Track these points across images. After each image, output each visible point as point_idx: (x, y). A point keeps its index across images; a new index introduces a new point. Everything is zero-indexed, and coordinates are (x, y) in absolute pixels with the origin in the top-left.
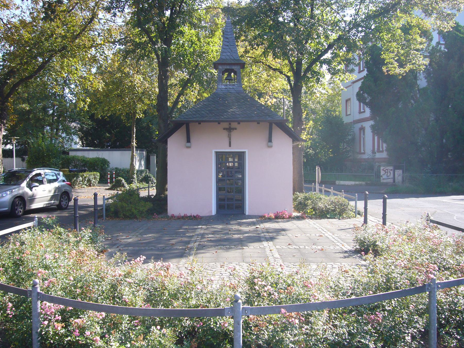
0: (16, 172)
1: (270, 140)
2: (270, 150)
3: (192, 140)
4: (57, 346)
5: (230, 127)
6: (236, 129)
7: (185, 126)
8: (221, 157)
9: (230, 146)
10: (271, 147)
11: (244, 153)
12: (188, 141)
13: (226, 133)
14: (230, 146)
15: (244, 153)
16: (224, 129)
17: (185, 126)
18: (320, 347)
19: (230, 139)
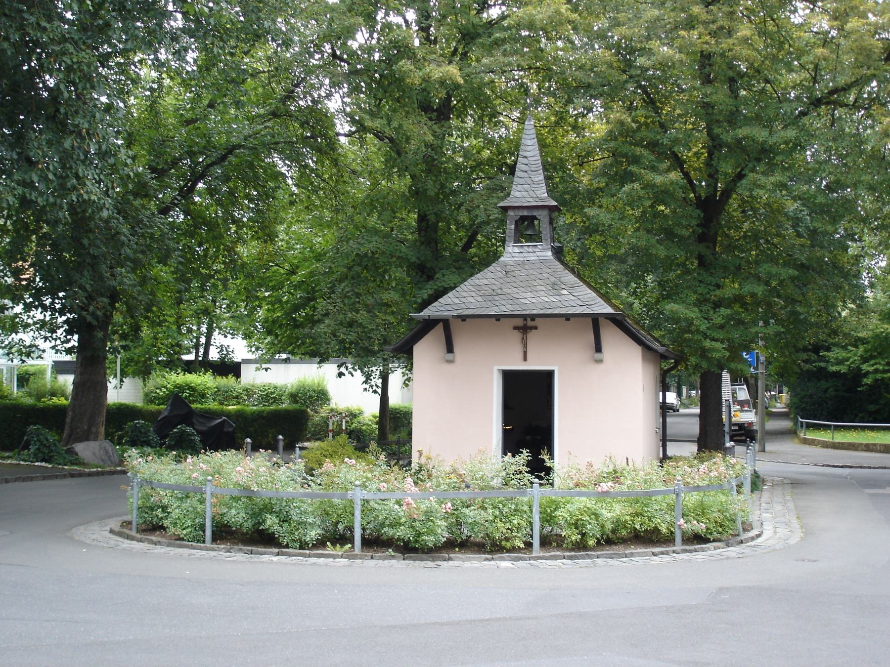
0: (419, 216)
1: (598, 349)
2: (600, 367)
3: (456, 349)
4: (597, 8)
5: (525, 325)
6: (536, 328)
7: (441, 325)
8: (511, 379)
9: (525, 359)
10: (600, 361)
11: (550, 374)
12: (450, 349)
13: (517, 335)
14: (525, 359)
15: (550, 374)
16: (515, 328)
17: (441, 325)
18: (475, 2)
19: (525, 346)
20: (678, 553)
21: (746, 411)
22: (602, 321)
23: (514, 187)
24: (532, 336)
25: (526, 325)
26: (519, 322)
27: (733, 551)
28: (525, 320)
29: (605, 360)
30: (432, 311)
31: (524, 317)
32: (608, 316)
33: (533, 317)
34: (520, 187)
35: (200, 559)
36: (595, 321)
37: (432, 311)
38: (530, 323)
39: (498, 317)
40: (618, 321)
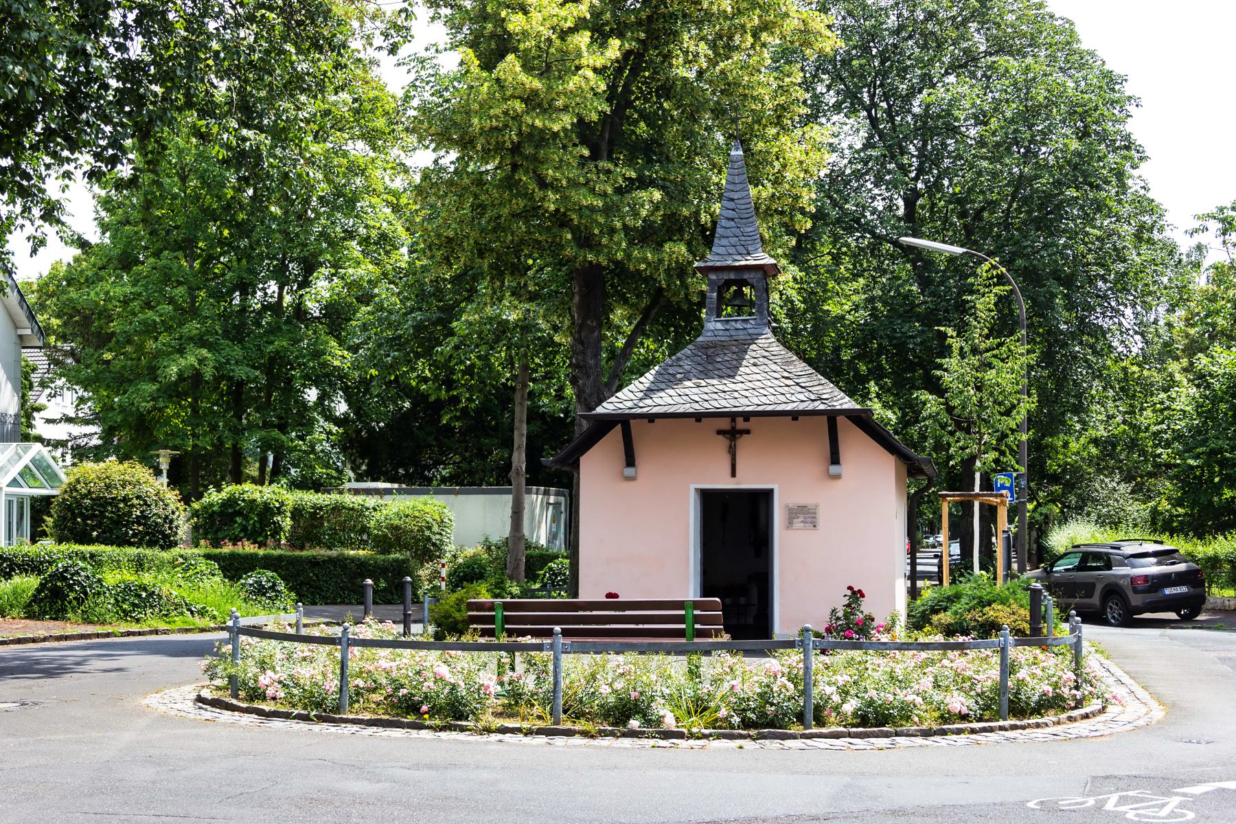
1: (835, 459)
6: (748, 432)
9: (733, 474)
12: (630, 461)
13: (723, 442)
14: (733, 474)
16: (719, 432)
20: (592, 737)
21: (633, 734)
22: (841, 420)
23: (716, 241)
24: (743, 443)
25: (734, 428)
26: (725, 424)
27: (1082, 727)
28: (733, 420)
29: (843, 476)
30: (607, 407)
31: (733, 416)
32: (851, 415)
33: (747, 416)
34: (724, 242)
35: (320, 734)
36: (832, 416)
37: (607, 407)
38: (741, 424)
39: (698, 417)
40: (862, 420)
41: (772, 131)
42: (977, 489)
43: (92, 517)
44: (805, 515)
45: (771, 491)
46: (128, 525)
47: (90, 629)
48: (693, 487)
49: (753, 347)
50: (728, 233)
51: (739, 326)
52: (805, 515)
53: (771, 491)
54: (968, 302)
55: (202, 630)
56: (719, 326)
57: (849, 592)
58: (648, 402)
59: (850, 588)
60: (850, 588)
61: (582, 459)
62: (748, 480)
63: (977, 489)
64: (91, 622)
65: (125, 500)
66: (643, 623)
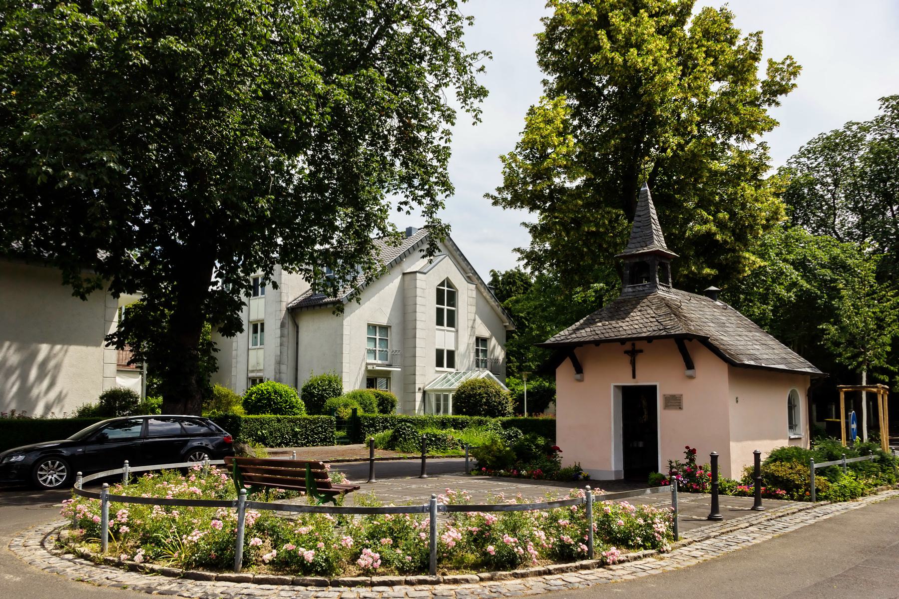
9: (634, 377)
13: (627, 358)
14: (634, 377)
25: (633, 349)
26: (628, 346)
34: (634, 241)
41: (422, 135)
42: (864, 384)
43: (464, 403)
44: (675, 402)
45: (655, 386)
46: (481, 406)
47: (402, 455)
48: (613, 384)
49: (645, 300)
50: (637, 235)
51: (641, 289)
52: (675, 402)
53: (655, 386)
54: (745, 258)
55: (438, 457)
56: (630, 290)
57: (687, 451)
58: (574, 336)
59: (687, 447)
60: (687, 447)
61: (557, 370)
62: (643, 380)
63: (864, 384)
64: (404, 452)
65: (480, 394)
66: (295, 471)
